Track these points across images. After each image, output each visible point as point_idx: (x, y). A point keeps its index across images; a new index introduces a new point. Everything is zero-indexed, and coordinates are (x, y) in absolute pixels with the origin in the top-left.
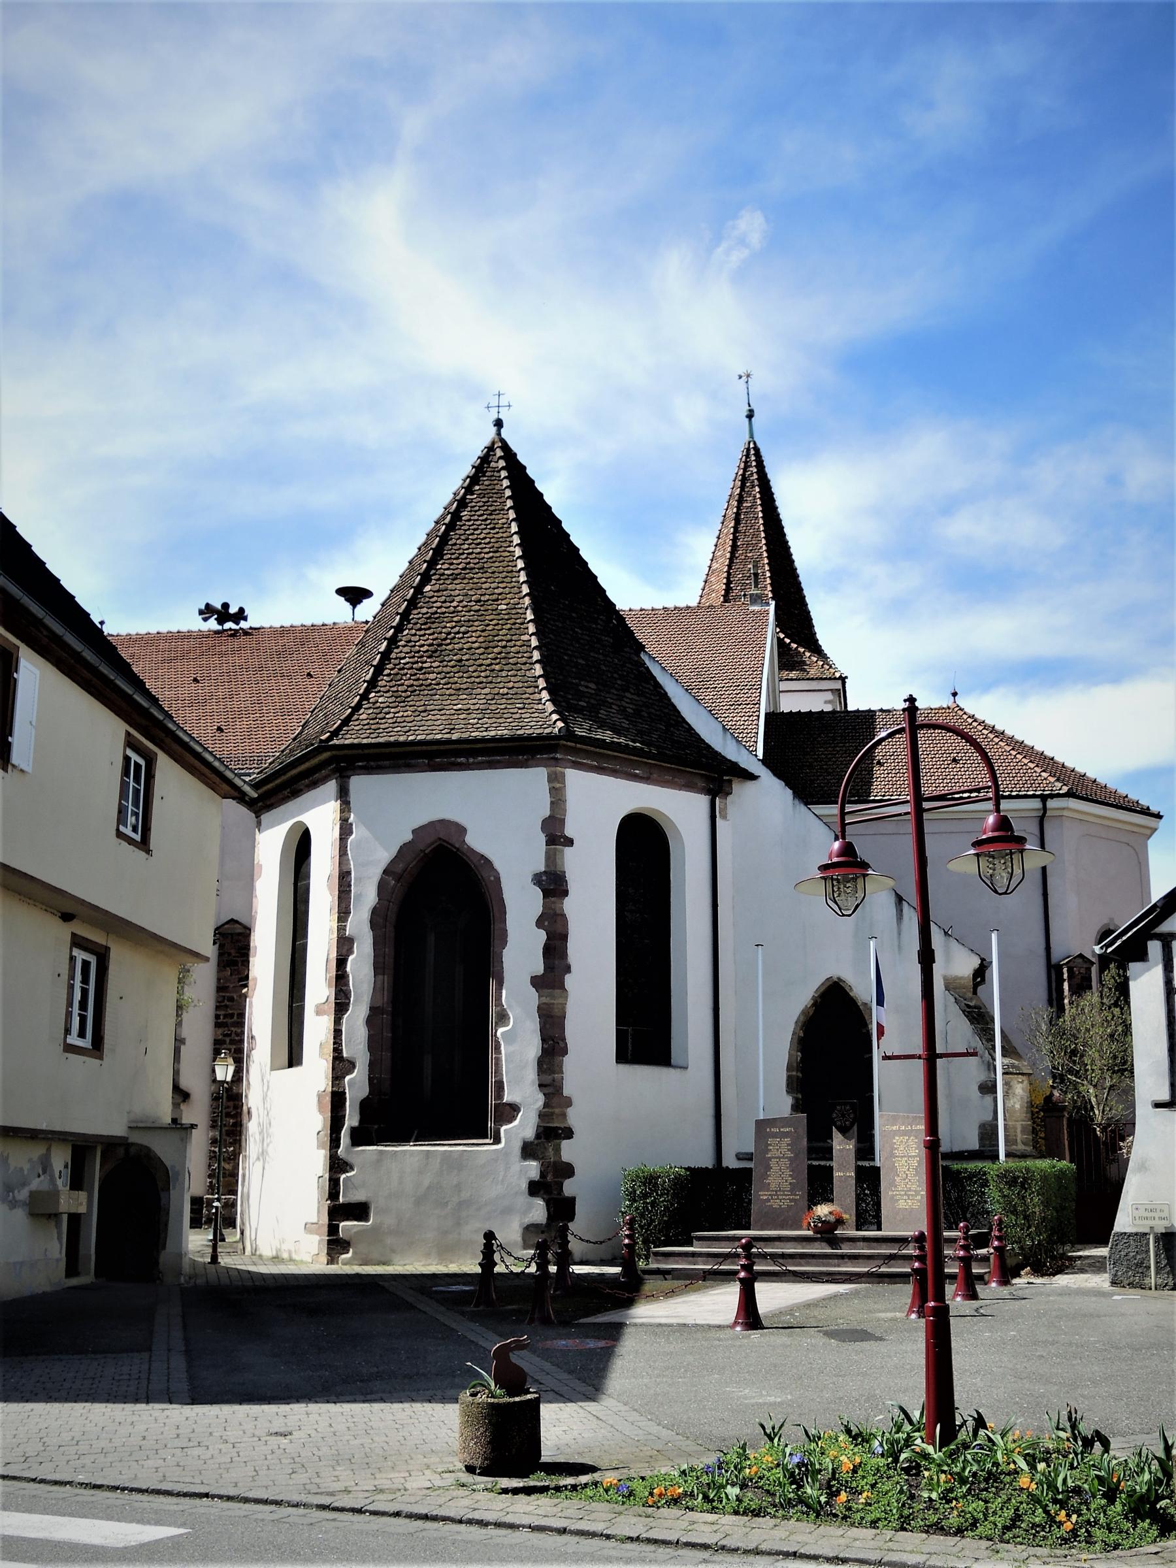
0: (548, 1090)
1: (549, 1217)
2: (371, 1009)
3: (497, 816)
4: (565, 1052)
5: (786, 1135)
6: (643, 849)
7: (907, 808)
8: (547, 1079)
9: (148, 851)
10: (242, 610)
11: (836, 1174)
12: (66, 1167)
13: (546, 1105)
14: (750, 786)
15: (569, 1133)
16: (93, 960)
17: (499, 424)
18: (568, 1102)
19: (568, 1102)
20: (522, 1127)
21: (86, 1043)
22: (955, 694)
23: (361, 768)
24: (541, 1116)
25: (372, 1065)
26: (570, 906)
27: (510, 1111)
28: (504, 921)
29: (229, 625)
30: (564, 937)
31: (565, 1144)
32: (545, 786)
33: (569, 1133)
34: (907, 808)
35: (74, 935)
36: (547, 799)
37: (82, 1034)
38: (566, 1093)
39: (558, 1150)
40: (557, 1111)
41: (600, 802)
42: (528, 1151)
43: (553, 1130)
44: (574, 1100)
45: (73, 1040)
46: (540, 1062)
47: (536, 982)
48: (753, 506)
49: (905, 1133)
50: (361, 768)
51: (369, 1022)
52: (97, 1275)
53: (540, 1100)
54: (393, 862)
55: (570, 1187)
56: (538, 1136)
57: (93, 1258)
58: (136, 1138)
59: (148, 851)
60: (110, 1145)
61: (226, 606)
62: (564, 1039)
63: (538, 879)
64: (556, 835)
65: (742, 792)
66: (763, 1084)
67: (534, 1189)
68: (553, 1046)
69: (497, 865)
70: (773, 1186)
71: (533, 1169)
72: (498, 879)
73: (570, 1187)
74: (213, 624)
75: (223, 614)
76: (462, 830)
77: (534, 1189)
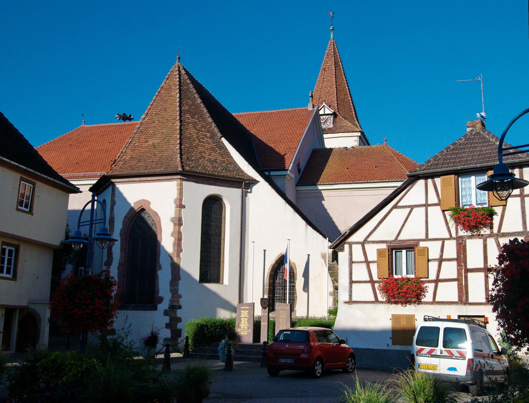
1: (171, 336)
4: (180, 279)
5: (247, 309)
6: (212, 208)
7: (89, 223)
8: (173, 288)
9: (32, 214)
11: (262, 324)
12: (2, 315)
13: (172, 297)
15: (180, 307)
18: (180, 296)
19: (180, 296)
20: (164, 306)
24: (171, 301)
27: (161, 300)
33: (180, 307)
34: (89, 223)
38: (179, 293)
39: (176, 313)
42: (166, 313)
44: (182, 295)
48: (331, 65)
51: (118, 268)
52: (16, 350)
53: (170, 295)
54: (128, 214)
55: (179, 326)
56: (169, 308)
57: (15, 345)
58: (32, 306)
59: (32, 214)
60: (22, 309)
62: (179, 275)
63: (172, 220)
65: (255, 188)
66: (256, 290)
67: (167, 326)
69: (159, 215)
70: (242, 328)
71: (167, 319)
73: (179, 326)
77: (167, 326)
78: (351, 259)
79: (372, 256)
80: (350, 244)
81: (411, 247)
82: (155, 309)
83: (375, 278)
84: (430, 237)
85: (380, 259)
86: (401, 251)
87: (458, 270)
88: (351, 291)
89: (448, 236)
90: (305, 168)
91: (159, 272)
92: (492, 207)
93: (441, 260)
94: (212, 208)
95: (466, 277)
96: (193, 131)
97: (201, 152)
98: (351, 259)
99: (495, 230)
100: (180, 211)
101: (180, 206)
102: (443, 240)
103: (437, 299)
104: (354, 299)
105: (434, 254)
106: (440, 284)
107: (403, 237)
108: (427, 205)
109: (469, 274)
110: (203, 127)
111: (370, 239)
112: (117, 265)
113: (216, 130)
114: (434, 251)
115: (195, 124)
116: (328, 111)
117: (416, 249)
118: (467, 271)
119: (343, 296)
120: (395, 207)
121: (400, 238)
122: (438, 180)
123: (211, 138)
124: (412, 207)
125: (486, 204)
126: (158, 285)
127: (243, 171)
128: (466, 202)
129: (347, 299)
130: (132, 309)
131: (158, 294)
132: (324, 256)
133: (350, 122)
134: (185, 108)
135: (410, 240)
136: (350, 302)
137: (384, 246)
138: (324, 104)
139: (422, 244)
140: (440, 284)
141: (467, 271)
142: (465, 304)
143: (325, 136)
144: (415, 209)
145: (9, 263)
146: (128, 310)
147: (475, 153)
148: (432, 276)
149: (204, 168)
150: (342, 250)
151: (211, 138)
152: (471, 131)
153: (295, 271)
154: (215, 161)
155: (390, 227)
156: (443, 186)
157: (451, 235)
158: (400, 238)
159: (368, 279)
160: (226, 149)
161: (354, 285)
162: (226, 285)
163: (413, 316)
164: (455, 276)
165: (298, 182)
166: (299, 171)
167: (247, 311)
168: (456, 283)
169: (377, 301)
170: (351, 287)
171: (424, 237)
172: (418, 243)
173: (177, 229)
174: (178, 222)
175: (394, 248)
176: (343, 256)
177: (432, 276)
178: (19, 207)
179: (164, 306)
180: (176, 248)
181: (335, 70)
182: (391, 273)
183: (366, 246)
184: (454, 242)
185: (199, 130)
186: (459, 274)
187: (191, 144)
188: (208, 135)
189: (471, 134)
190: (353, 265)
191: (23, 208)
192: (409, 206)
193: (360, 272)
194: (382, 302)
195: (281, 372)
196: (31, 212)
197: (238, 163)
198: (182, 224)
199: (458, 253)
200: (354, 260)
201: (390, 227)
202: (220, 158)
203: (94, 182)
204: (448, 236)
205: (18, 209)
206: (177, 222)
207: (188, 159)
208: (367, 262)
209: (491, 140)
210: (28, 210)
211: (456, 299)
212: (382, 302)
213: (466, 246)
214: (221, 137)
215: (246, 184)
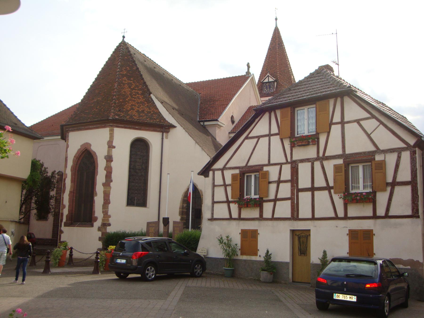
0: (105, 213)
2: (70, 192)
3: (97, 139)
4: (109, 203)
5: (153, 226)
6: (140, 149)
8: (104, 210)
13: (104, 217)
14: (175, 129)
15: (109, 225)
17: (124, 37)
18: (110, 216)
19: (110, 216)
23: (71, 130)
24: (103, 220)
25: (69, 206)
26: (113, 164)
28: (97, 168)
30: (111, 173)
31: (108, 227)
32: (108, 133)
33: (109, 225)
36: (109, 136)
38: (109, 214)
39: (106, 229)
40: (106, 219)
41: (124, 137)
43: (105, 224)
44: (112, 216)
46: (103, 206)
50: (71, 130)
51: (69, 195)
56: (101, 225)
64: (111, 146)
65: (173, 131)
68: (107, 201)
69: (97, 154)
71: (100, 234)
72: (97, 158)
78: (214, 183)
79: (229, 181)
80: (214, 171)
84: (272, 162)
87: (292, 190)
93: (279, 182)
94: (140, 149)
97: (132, 105)
98: (214, 183)
99: (321, 155)
101: (111, 146)
102: (281, 164)
103: (275, 216)
104: (215, 217)
105: (274, 177)
106: (278, 203)
108: (270, 135)
111: (228, 166)
112: (69, 193)
114: (273, 173)
115: (130, 85)
120: (247, 138)
121: (250, 164)
122: (278, 112)
124: (259, 137)
126: (94, 208)
127: (165, 119)
128: (301, 131)
130: (77, 226)
131: (94, 215)
136: (212, 219)
137: (237, 171)
139: (265, 169)
140: (278, 203)
144: (261, 139)
146: (74, 227)
148: (272, 196)
156: (282, 118)
157: (287, 160)
158: (248, 165)
163: (256, 231)
164: (289, 196)
168: (289, 202)
169: (231, 218)
170: (213, 207)
171: (267, 162)
172: (263, 168)
175: (245, 172)
177: (272, 196)
179: (98, 224)
184: (289, 166)
185: (133, 89)
186: (292, 193)
188: (140, 92)
194: (235, 219)
195: (130, 276)
202: (147, 110)
207: (119, 110)
208: (225, 186)
211: (289, 216)
212: (235, 219)
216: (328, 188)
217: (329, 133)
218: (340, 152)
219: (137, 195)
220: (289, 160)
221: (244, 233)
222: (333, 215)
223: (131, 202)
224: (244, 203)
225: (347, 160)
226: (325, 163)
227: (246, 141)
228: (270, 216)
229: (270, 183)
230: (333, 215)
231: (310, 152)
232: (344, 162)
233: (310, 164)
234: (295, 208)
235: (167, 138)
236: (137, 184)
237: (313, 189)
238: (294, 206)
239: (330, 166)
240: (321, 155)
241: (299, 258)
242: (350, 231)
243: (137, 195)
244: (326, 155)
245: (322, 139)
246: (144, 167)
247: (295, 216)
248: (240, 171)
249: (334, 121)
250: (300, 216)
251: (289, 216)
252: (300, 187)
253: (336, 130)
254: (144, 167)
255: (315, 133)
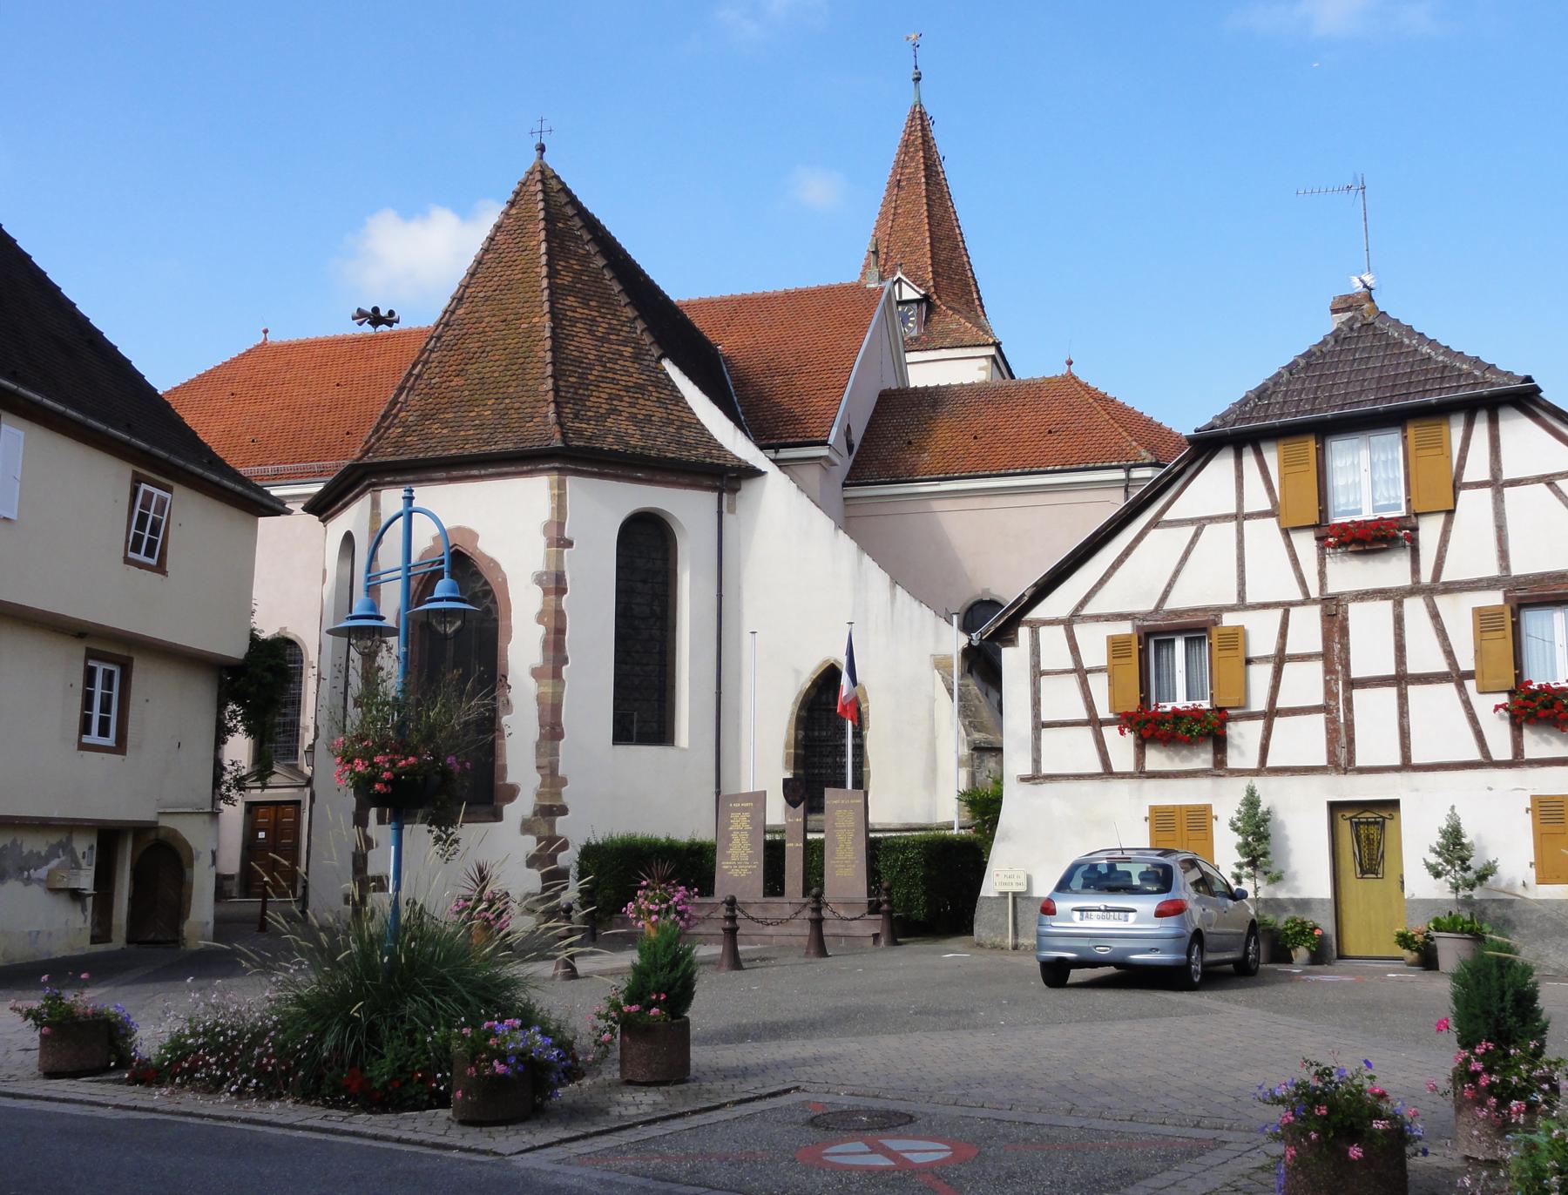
3: (506, 519)
5: (745, 809)
6: (646, 551)
7: (399, 573)
9: (164, 573)
10: (391, 313)
12: (91, 848)
14: (757, 482)
15: (563, 811)
16: (116, 670)
19: (564, 782)
21: (110, 741)
22: (1070, 363)
27: (512, 793)
29: (383, 328)
31: (559, 819)
34: (399, 573)
35: (88, 650)
37: (104, 732)
39: (552, 826)
41: (601, 506)
42: (527, 827)
43: (550, 810)
45: (94, 738)
47: (536, 673)
49: (844, 807)
52: (129, 941)
53: (536, 779)
56: (535, 814)
58: (164, 822)
59: (164, 573)
60: (140, 830)
61: (376, 310)
63: (539, 579)
65: (749, 488)
66: (764, 762)
67: (532, 862)
68: (552, 730)
69: (504, 567)
71: (530, 844)
72: (505, 581)
74: (367, 329)
75: (375, 318)
76: (474, 536)
77: (532, 862)
80: (1035, 626)
81: (1197, 629)
82: (497, 816)
83: (1104, 712)
84: (1250, 599)
85: (1117, 661)
86: (1173, 641)
87: (1327, 683)
88: (1037, 749)
89: (1300, 597)
90: (864, 439)
91: (505, 720)
92: (1417, 515)
93: (1280, 659)
94: (646, 551)
95: (1349, 702)
96: (587, 342)
99: (1426, 577)
100: (560, 557)
101: (559, 541)
102: (1286, 606)
104: (1046, 769)
106: (1278, 721)
107: (1175, 602)
108: (1240, 517)
109: (1357, 694)
110: (611, 328)
111: (1089, 610)
113: (647, 339)
114: (1261, 634)
116: (909, 293)
117: (1215, 632)
118: (1352, 684)
119: (1016, 762)
120: (1155, 523)
123: (636, 357)
124: (1200, 523)
125: (1398, 507)
126: (503, 756)
127: (721, 446)
129: (1028, 770)
131: (504, 778)
132: (941, 665)
133: (968, 319)
134: (566, 279)
135: (1196, 610)
136: (1036, 777)
137: (1126, 628)
138: (899, 274)
141: (1352, 684)
142: (1346, 771)
143: (910, 357)
145: (106, 707)
147: (1368, 375)
148: (1259, 703)
149: (619, 438)
150: (1012, 642)
151: (636, 357)
152: (1349, 319)
153: (864, 706)
154: (648, 419)
155: (1140, 577)
156: (1285, 464)
158: (1168, 606)
159: (1084, 716)
160: (675, 388)
161: (1046, 734)
162: (684, 750)
164: (1319, 700)
165: (849, 477)
166: (850, 447)
167: (747, 815)
168: (1320, 718)
169: (1108, 773)
170: (1037, 739)
171: (1234, 600)
173: (553, 604)
174: (555, 585)
175: (1154, 636)
176: (1013, 660)
177: (1259, 703)
178: (131, 555)
179: (518, 810)
180: (551, 654)
181: (927, 184)
182: (1145, 700)
183: (1078, 629)
184: (1315, 612)
185: (604, 339)
186: (1330, 693)
187: (582, 376)
188: (628, 351)
189: (1352, 329)
190: (1044, 680)
191: (141, 557)
192: (1191, 521)
193: (1062, 699)
194: (1123, 776)
196: (160, 568)
197: (707, 426)
198: (564, 591)
199: (1327, 638)
200: (1043, 667)
201: (1140, 577)
202: (659, 414)
203: (316, 488)
204: (1300, 597)
205: (127, 561)
206: (552, 586)
207: (576, 416)
209: (1406, 341)
210: (153, 562)
211: (1323, 761)
212: (1123, 776)
213: (1346, 619)
214: (660, 358)
215: (729, 478)
216: (1457, 677)
217: (1450, 513)
218: (1493, 570)
219: (643, 710)
220: (1314, 593)
221: (1161, 819)
222: (1475, 755)
223: (622, 734)
224: (1153, 728)
225: (1519, 594)
226: (1442, 602)
227: (1154, 533)
228: (1253, 763)
229: (1249, 661)
230: (1475, 755)
231: (1392, 570)
232: (1506, 599)
233: (1389, 604)
234: (1341, 740)
235: (732, 511)
236: (638, 668)
237: (1401, 680)
238: (1337, 731)
239: (1459, 613)
240: (1426, 577)
241: (1354, 885)
242: (1153, 809)
243: (643, 710)
244: (1445, 577)
245: (1429, 531)
246: (657, 609)
247: (1341, 757)
248: (1138, 628)
249: (1467, 477)
250: (1360, 762)
251: (1323, 761)
252: (1355, 674)
253: (1474, 506)
254: (657, 609)
255: (1402, 512)
